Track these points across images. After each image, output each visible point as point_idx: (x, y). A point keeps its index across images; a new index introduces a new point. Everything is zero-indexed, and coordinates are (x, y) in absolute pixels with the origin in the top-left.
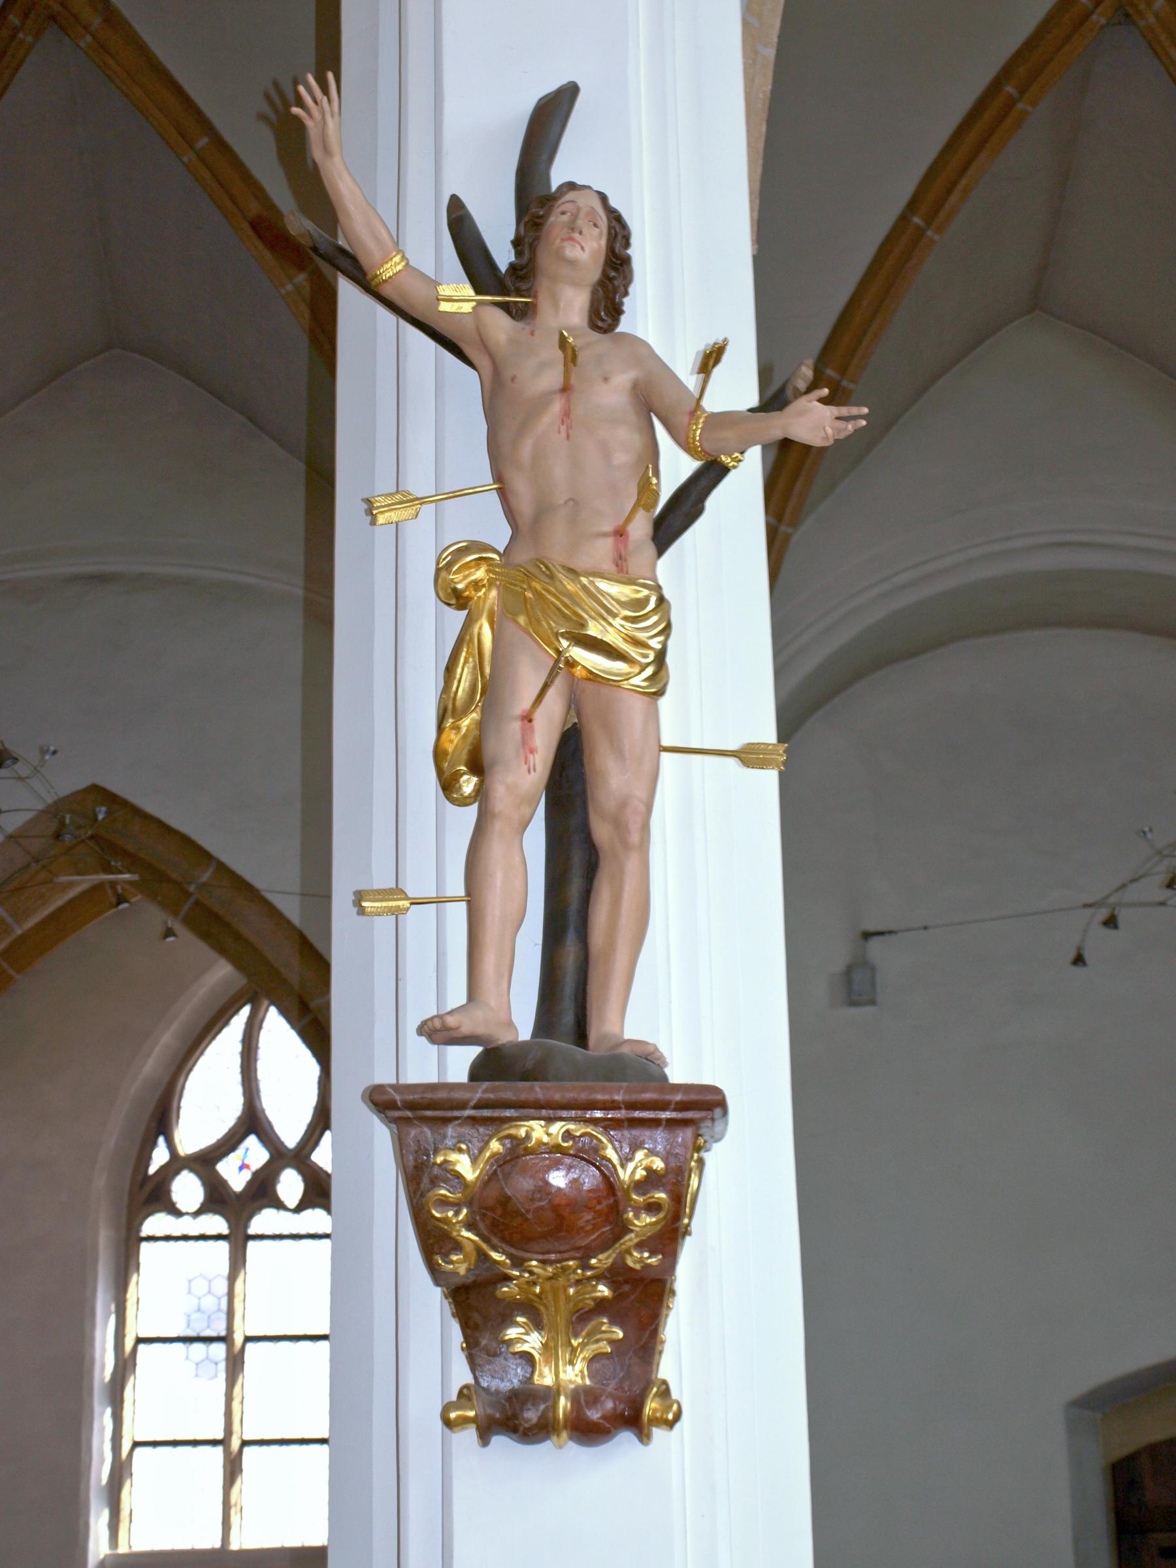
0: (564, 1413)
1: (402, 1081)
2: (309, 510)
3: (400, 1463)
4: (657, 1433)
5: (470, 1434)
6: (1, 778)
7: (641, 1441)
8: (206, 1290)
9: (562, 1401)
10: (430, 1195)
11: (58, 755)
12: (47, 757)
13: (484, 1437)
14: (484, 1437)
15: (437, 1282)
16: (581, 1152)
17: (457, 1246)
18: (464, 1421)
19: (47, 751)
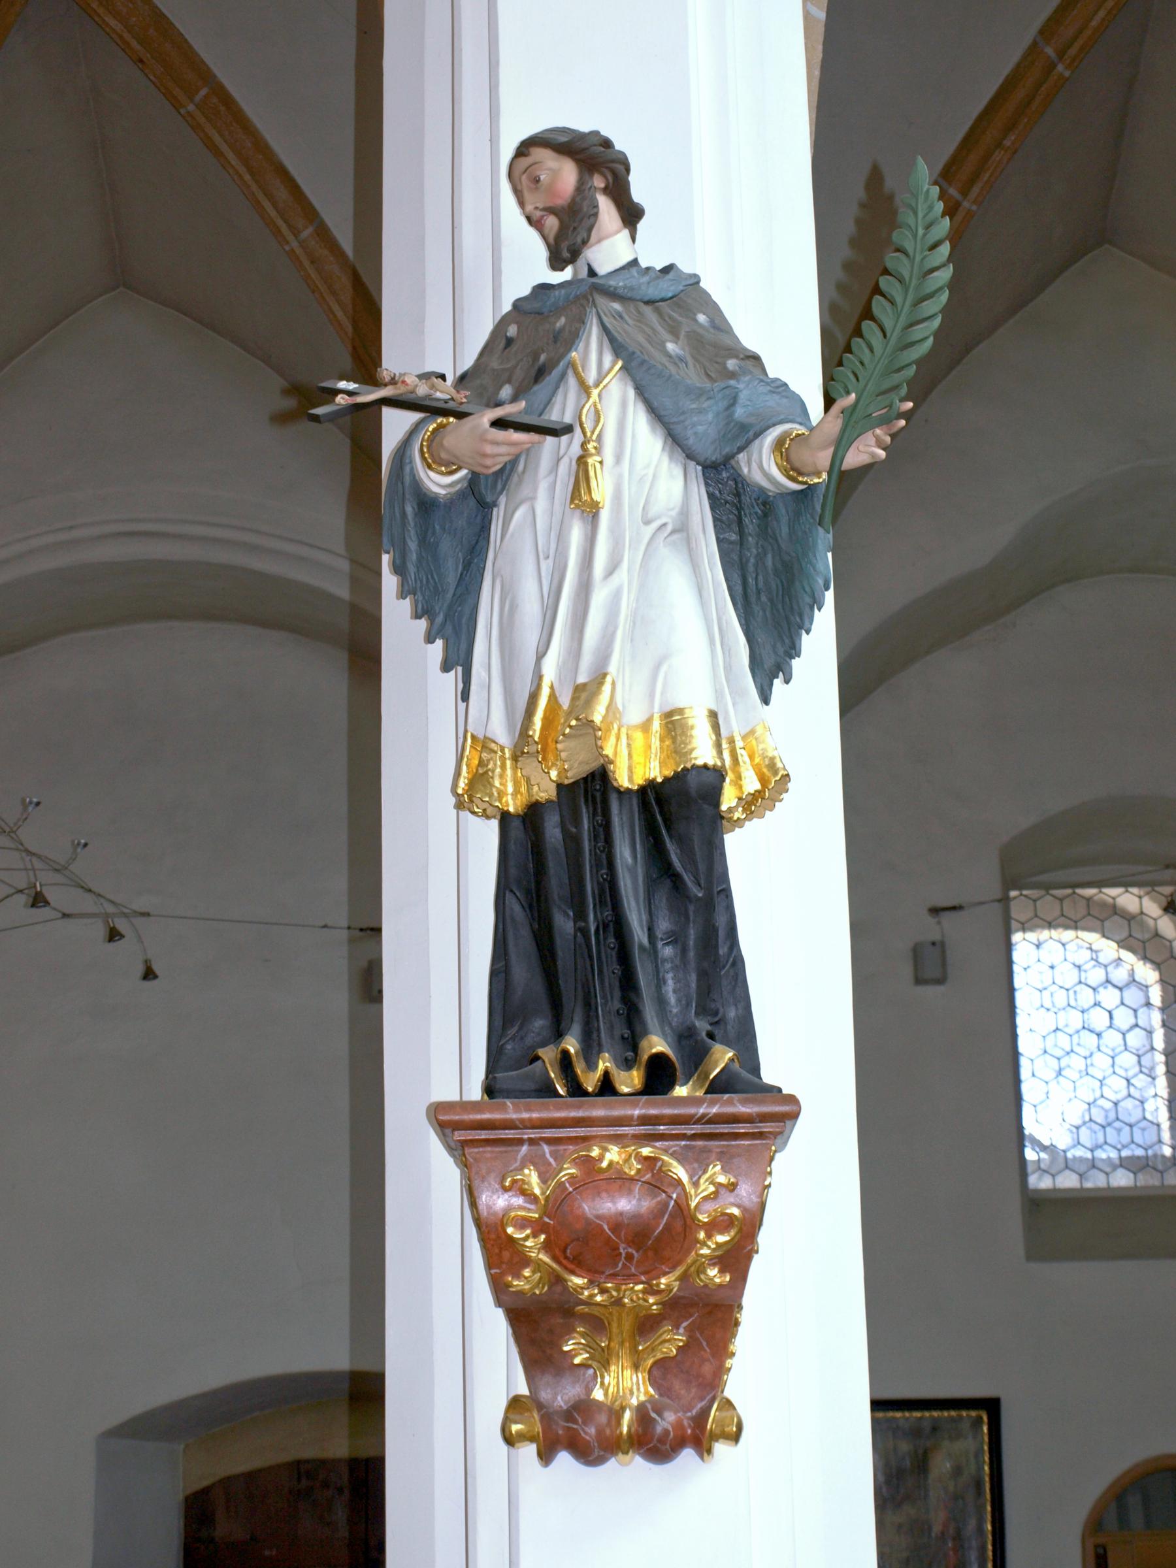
0: (629, 1428)
1: (465, 1099)
2: (355, 468)
3: (468, 1476)
4: (720, 1448)
5: (529, 1451)
6: (3, 900)
7: (702, 1458)
8: (1118, 1002)
9: (627, 1416)
10: (485, 1214)
11: (89, 846)
12: (79, 850)
13: (546, 1456)
14: (546, 1456)
15: (499, 1303)
16: (546, 1193)
17: (526, 1261)
18: (523, 1437)
19: (79, 844)
